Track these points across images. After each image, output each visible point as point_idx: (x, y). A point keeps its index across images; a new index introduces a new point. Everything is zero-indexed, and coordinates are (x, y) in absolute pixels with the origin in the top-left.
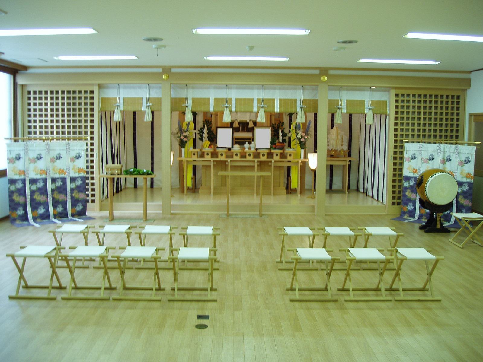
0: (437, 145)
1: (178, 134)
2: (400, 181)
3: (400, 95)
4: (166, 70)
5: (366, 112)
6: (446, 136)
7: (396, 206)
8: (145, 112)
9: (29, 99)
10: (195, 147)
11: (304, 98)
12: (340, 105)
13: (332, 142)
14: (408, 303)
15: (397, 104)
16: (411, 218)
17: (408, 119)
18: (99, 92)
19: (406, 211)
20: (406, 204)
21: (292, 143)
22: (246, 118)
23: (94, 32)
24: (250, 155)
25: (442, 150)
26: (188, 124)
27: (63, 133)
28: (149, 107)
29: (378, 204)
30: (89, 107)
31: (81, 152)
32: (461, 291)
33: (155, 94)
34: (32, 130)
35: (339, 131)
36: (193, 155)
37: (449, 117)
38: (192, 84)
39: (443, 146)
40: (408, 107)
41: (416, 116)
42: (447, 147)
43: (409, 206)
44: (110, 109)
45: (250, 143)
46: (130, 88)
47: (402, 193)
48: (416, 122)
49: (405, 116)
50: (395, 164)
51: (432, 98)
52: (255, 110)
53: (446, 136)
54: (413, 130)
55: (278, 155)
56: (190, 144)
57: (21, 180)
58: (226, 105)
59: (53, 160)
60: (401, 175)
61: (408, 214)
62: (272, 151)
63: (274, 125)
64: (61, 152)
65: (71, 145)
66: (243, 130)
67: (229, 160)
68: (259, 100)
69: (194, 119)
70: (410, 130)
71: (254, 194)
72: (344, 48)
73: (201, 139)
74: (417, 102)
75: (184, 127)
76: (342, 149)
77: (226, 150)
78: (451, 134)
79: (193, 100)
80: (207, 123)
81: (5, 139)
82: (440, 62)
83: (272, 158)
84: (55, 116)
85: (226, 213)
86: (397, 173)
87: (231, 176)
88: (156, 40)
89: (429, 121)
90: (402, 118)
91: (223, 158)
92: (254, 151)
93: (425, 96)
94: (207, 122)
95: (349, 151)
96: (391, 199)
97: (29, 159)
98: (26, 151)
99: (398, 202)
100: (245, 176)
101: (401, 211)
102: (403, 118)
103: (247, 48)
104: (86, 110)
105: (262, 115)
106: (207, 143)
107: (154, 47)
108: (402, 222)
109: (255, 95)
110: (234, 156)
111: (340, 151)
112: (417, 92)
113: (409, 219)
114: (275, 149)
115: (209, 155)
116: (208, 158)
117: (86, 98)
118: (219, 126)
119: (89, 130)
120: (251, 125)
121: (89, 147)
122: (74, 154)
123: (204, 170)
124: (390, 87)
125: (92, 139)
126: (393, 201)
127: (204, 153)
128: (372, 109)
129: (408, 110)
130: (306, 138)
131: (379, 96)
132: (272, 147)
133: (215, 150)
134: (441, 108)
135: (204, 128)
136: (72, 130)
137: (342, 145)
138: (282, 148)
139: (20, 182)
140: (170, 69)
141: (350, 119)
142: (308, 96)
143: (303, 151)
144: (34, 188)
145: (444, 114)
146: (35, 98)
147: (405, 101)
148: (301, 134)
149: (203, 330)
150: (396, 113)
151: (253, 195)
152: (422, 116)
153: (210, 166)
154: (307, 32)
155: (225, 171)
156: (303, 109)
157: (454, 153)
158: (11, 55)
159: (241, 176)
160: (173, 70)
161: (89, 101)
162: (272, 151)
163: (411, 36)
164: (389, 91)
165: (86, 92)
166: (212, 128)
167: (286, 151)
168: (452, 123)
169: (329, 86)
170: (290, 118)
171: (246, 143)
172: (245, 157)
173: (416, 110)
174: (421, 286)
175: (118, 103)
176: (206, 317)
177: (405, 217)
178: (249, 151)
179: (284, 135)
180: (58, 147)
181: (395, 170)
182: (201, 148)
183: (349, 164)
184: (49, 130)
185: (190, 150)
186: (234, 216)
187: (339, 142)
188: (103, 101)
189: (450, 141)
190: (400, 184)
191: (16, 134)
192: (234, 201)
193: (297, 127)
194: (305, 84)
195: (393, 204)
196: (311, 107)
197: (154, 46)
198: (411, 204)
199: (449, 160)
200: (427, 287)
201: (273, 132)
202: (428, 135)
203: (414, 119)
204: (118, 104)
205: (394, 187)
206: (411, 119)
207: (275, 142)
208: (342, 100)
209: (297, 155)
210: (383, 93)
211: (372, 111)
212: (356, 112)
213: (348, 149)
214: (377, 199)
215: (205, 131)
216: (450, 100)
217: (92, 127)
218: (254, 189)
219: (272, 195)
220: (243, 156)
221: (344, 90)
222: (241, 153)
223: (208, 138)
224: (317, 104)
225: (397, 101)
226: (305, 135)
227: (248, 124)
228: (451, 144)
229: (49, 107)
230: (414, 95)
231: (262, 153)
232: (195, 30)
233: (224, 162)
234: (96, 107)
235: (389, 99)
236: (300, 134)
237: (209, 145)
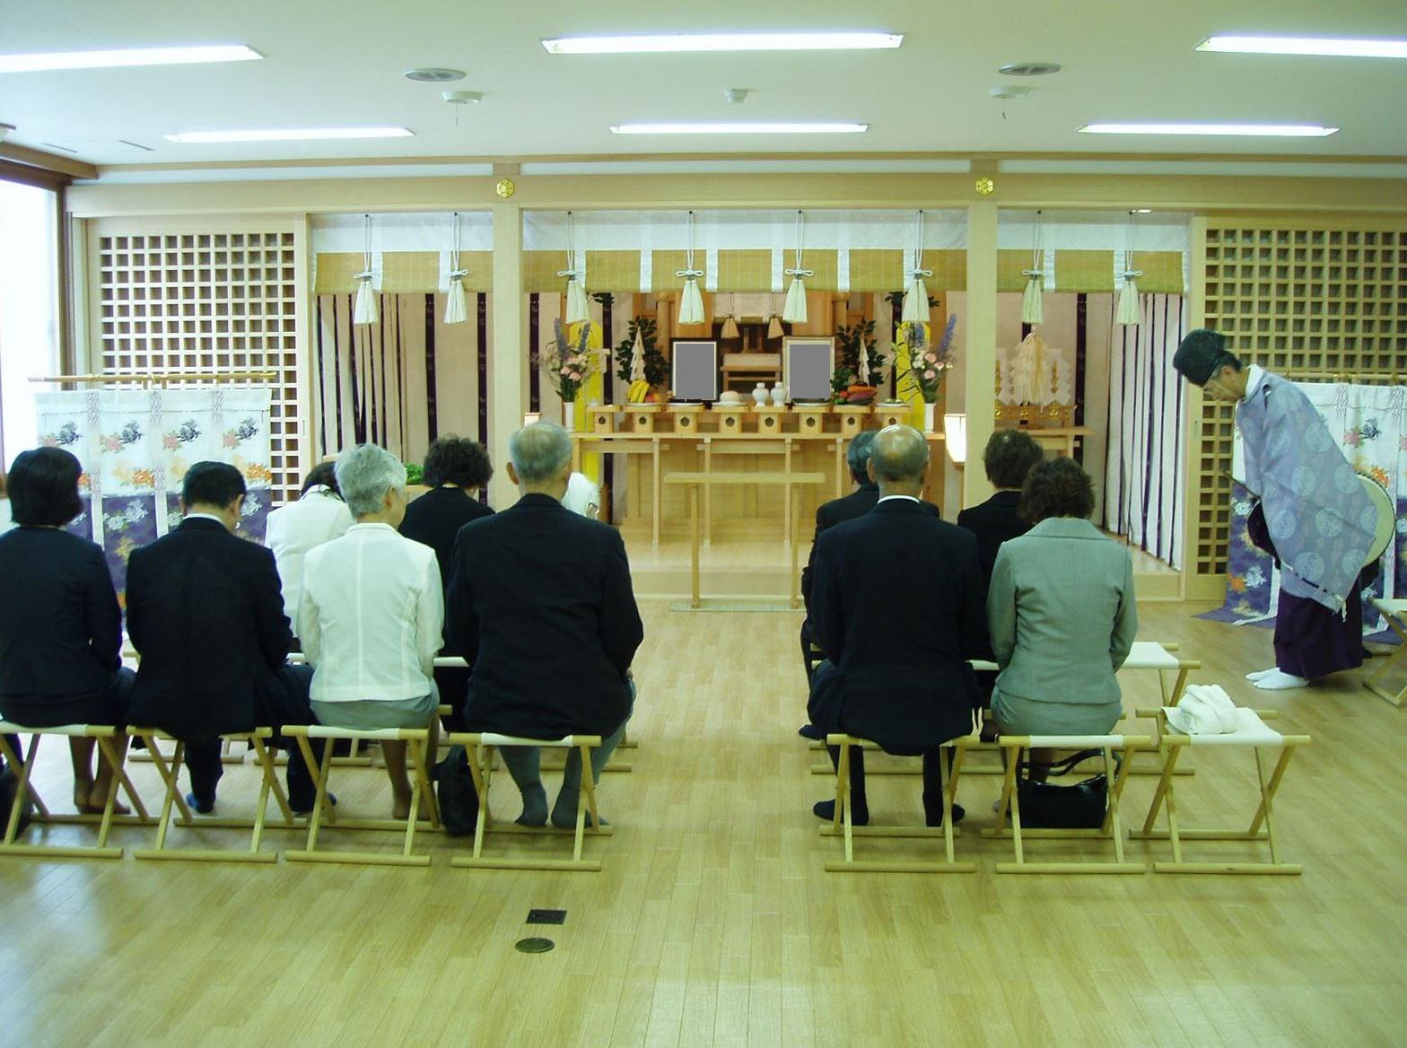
0: (1335, 385)
1: (554, 360)
2: (1224, 498)
3: (1222, 234)
4: (508, 169)
5: (1117, 287)
6: (1368, 360)
7: (1212, 577)
8: (445, 295)
9: (107, 260)
10: (608, 397)
11: (926, 248)
12: (1036, 267)
13: (1022, 381)
14: (1196, 880)
15: (1212, 262)
16: (1256, 614)
17: (1247, 306)
18: (312, 238)
19: (1241, 590)
20: (1243, 570)
21: (900, 385)
22: (761, 312)
23: (254, 56)
24: (769, 422)
25: (1352, 400)
26: (585, 332)
27: (190, 360)
28: (459, 282)
29: (1158, 568)
30: (280, 282)
31: (256, 416)
32: (1371, 843)
33: (476, 240)
34: (117, 353)
35: (1044, 348)
36: (598, 425)
37: (1377, 299)
38: (586, 209)
39: (1354, 388)
40: (1248, 270)
41: (1273, 297)
42: (1366, 391)
43: (1250, 577)
44: (342, 289)
45: (770, 386)
46: (403, 223)
47: (1229, 536)
48: (1273, 315)
49: (1238, 297)
50: (1207, 446)
51: (1322, 242)
52: (777, 284)
53: (1368, 360)
54: (1299, 342)
55: (856, 421)
56: (591, 393)
57: (142, 498)
58: (690, 272)
59: (172, 442)
60: (1226, 480)
61: (1246, 599)
62: (838, 409)
63: (843, 330)
64: (197, 418)
65: (225, 396)
66: (753, 348)
67: (707, 438)
68: (788, 256)
69: (607, 316)
70: (1290, 342)
71: (782, 541)
72: (1019, 90)
73: (626, 375)
74: (1274, 253)
75: (574, 340)
76: (1055, 401)
77: (697, 408)
78: (1384, 353)
79: (593, 259)
80: (641, 326)
81: (30, 380)
82: (1337, 130)
83: (838, 430)
84: (214, 309)
85: (691, 596)
86: (1215, 473)
87: (712, 486)
88: (444, 75)
89: (1347, 313)
90: (1230, 305)
91: (687, 432)
92: (782, 411)
93: (1301, 235)
94: (645, 324)
95: (1076, 407)
96: (1197, 554)
97: (102, 438)
98: (94, 415)
99: (1217, 564)
100: (756, 486)
101: (1228, 592)
102: (1233, 303)
103: (727, 94)
104: (271, 290)
105: (796, 299)
106: (640, 385)
107: (446, 99)
108: (1226, 625)
109: (777, 239)
110: (723, 425)
111: (1047, 409)
112: (1275, 225)
113: (1251, 614)
114: (845, 403)
115: (605, 425)
116: (643, 431)
117: (271, 256)
118: (678, 335)
119: (282, 351)
120: (775, 331)
121: (283, 402)
122: (234, 423)
123: (633, 470)
124: (1188, 210)
125: (291, 376)
126: (1204, 559)
127: (630, 416)
128: (1137, 277)
129: (1247, 281)
130: (940, 368)
131: (1154, 239)
132: (837, 397)
133: (664, 408)
134: (1352, 272)
135: (633, 343)
136: (231, 351)
137: (1054, 390)
138: (868, 400)
139: (138, 505)
140: (519, 165)
141: (1081, 309)
142: (939, 240)
143: (930, 408)
144: (117, 523)
145: (1361, 290)
146: (123, 259)
147: (1239, 253)
148: (924, 359)
149: (535, 956)
150: (1211, 288)
151: (781, 542)
152: (1360, 299)
153: (651, 456)
154: (894, 42)
155: (698, 472)
156: (924, 282)
157: (1386, 410)
158: (38, 131)
159: (746, 486)
160: (528, 169)
161: (279, 265)
162: (838, 409)
163: (1220, 44)
164: (1187, 222)
165: (271, 238)
166: (659, 340)
167: (878, 410)
168: (1386, 318)
169: (1000, 208)
170: (534, 310)
171: (759, 385)
172: (755, 428)
173: (1273, 279)
174: (1244, 827)
175: (367, 269)
176: (555, 917)
177: (1240, 609)
178: (767, 409)
179: (876, 361)
180: (188, 402)
181: (1207, 464)
182: (622, 402)
183: (1075, 449)
184: (166, 352)
185: (590, 410)
186: (712, 608)
187: (1045, 379)
188: (324, 263)
189: (1363, 373)
190: (1223, 508)
191: (67, 366)
192: (712, 559)
193: (915, 336)
194: (932, 203)
195: (1203, 568)
196: (947, 274)
197: (446, 96)
198: (1257, 570)
199: (1373, 433)
200: (1263, 830)
201: (841, 353)
202: (1312, 356)
203: (1265, 306)
204: (368, 274)
205: (1205, 516)
206: (1255, 306)
207: (846, 383)
208: (1042, 251)
209: (915, 420)
210: (1168, 228)
211: (1136, 284)
212: (1095, 288)
213: (1074, 400)
214: (1155, 554)
215: (638, 350)
216: (1379, 247)
217: (290, 342)
218: (782, 526)
219: (656, 541)
220: (749, 425)
221: (1047, 220)
222: (743, 416)
223: (644, 372)
224: (964, 265)
225: (1212, 252)
226: (937, 361)
227: (766, 327)
228: (1385, 383)
229: (180, 284)
230: (1266, 234)
231: (727, 417)
232: (553, 43)
233: (690, 444)
234: (300, 282)
235: (1187, 245)
236: (920, 357)
237: (648, 394)
